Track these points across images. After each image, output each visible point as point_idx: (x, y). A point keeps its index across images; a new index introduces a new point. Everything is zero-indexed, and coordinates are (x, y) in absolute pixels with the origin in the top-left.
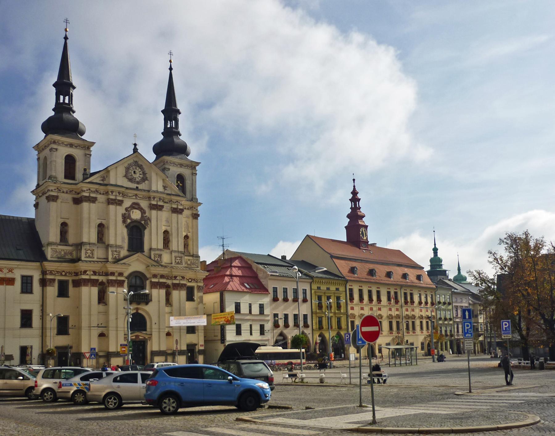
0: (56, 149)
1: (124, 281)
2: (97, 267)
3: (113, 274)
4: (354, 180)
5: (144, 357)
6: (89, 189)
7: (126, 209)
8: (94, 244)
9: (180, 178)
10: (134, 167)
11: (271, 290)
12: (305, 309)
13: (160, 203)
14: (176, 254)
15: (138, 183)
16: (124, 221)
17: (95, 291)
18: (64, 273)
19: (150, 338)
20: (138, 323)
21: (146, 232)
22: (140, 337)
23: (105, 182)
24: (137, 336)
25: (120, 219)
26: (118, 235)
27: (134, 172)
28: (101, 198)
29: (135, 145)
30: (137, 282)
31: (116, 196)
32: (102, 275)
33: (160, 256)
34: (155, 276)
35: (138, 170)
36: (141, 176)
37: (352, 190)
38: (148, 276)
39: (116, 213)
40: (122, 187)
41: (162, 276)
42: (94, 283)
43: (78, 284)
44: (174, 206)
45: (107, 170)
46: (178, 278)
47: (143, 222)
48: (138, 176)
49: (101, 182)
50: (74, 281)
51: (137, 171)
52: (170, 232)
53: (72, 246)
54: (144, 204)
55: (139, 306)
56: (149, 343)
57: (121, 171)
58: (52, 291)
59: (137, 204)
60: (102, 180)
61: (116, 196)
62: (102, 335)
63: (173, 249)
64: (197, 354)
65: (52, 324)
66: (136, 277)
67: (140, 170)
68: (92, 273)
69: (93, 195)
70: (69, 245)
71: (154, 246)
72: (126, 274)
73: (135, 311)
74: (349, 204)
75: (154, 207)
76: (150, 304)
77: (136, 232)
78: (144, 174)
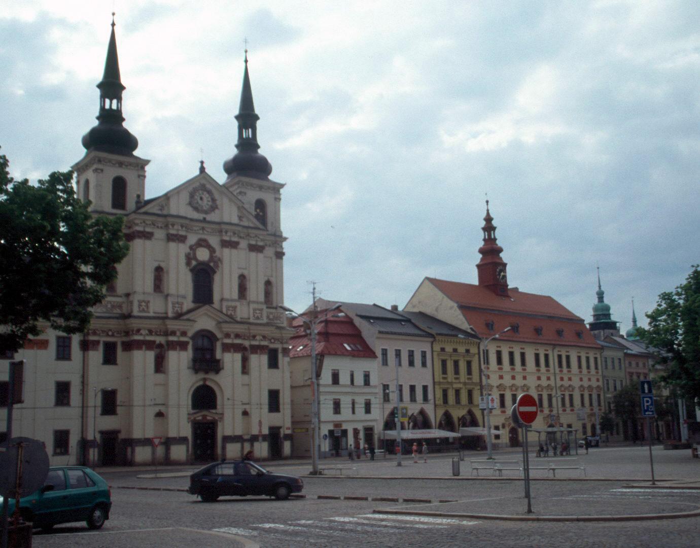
0: (102, 170)
1: (187, 343)
2: (154, 325)
3: (173, 333)
4: (487, 202)
5: (213, 445)
6: (144, 222)
7: (191, 248)
8: (149, 294)
9: (260, 205)
10: (201, 192)
11: (379, 353)
12: (421, 376)
13: (235, 239)
14: (255, 306)
15: (206, 212)
16: (188, 263)
17: (150, 356)
18: (110, 333)
19: (222, 419)
20: (204, 398)
21: (217, 278)
22: (208, 418)
23: (165, 212)
24: (204, 417)
25: (183, 260)
26: (181, 283)
27: (201, 199)
28: (160, 234)
29: (202, 163)
30: (205, 361)
31: (230, 236)
32: (160, 335)
33: (235, 308)
34: (227, 335)
35: (206, 196)
36: (210, 203)
37: (484, 215)
38: (219, 335)
39: (179, 251)
40: (186, 218)
41: (237, 336)
42: (150, 345)
43: (129, 346)
44: (253, 242)
45: (167, 196)
46: (142, 332)
47: (212, 264)
48: (206, 203)
49: (159, 212)
50: (123, 343)
51: (203, 196)
52: (248, 278)
53: (121, 297)
54: (214, 241)
55: (206, 376)
56: (220, 424)
57: (185, 197)
58: (96, 356)
59: (205, 241)
60: (161, 210)
61: (178, 230)
62: (160, 415)
63: (252, 299)
64: (282, 440)
65: (95, 401)
66: (203, 336)
67: (207, 195)
68: (147, 332)
69: (148, 230)
70: (118, 296)
71: (227, 295)
72: (190, 334)
73: (201, 383)
74: (481, 235)
75: (225, 244)
76: (222, 373)
77: (203, 277)
78: (214, 200)
